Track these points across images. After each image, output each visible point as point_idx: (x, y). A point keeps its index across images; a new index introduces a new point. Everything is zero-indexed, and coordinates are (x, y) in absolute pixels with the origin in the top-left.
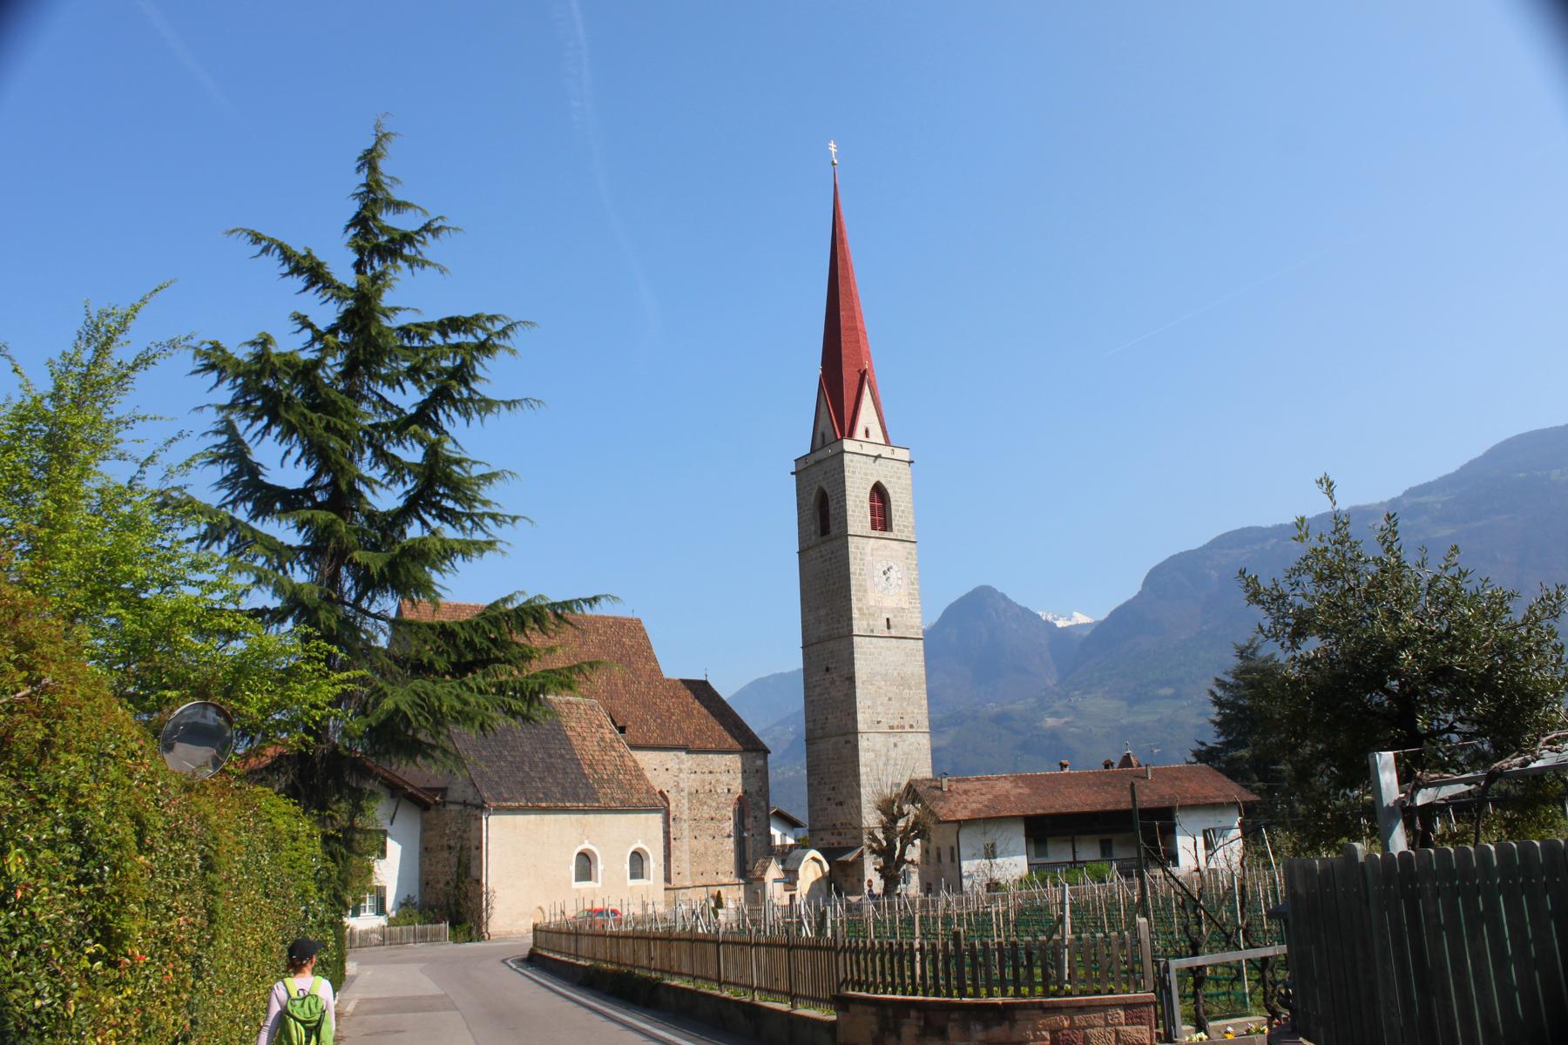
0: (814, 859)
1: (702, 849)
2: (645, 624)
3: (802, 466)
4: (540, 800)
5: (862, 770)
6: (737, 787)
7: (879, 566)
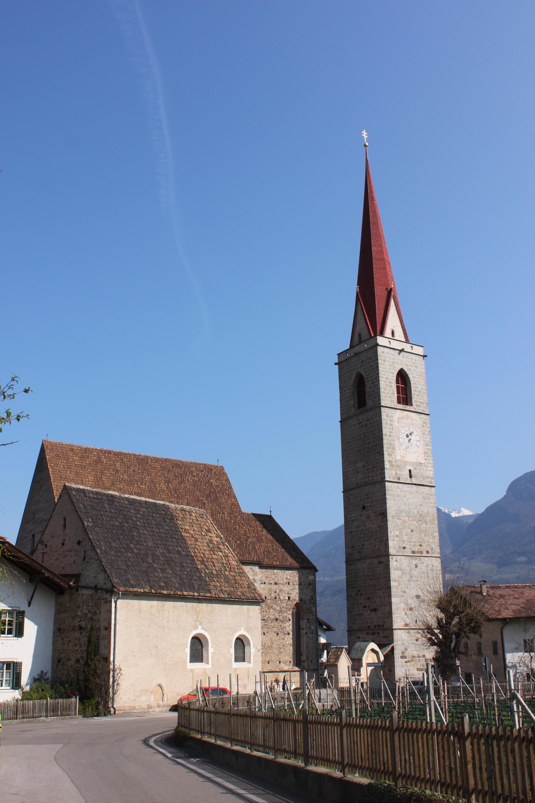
0: (373, 650)
1: (269, 643)
2: (226, 471)
3: (343, 358)
4: (162, 588)
5: (393, 584)
6: (295, 595)
7: (403, 431)
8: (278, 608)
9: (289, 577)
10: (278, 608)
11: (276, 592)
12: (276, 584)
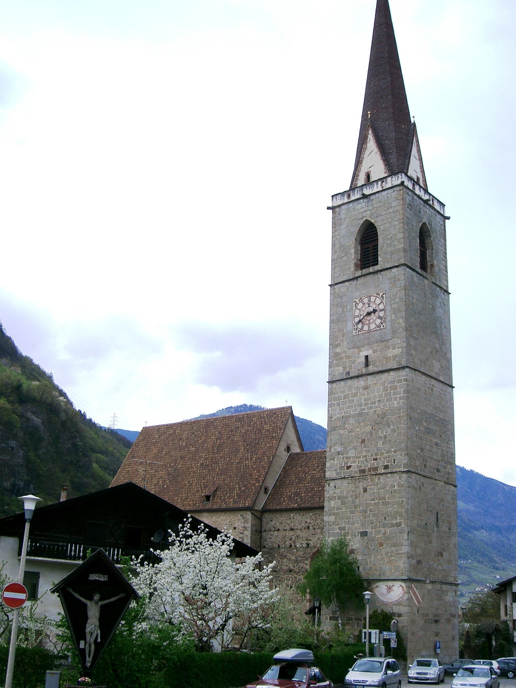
8: (293, 558)
9: (308, 521)
10: (293, 558)
11: (291, 539)
12: (292, 529)
